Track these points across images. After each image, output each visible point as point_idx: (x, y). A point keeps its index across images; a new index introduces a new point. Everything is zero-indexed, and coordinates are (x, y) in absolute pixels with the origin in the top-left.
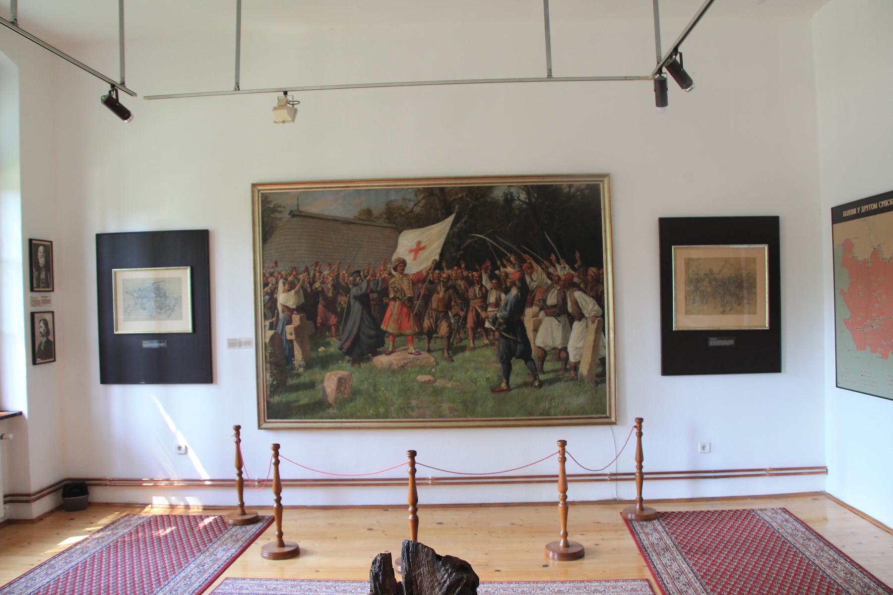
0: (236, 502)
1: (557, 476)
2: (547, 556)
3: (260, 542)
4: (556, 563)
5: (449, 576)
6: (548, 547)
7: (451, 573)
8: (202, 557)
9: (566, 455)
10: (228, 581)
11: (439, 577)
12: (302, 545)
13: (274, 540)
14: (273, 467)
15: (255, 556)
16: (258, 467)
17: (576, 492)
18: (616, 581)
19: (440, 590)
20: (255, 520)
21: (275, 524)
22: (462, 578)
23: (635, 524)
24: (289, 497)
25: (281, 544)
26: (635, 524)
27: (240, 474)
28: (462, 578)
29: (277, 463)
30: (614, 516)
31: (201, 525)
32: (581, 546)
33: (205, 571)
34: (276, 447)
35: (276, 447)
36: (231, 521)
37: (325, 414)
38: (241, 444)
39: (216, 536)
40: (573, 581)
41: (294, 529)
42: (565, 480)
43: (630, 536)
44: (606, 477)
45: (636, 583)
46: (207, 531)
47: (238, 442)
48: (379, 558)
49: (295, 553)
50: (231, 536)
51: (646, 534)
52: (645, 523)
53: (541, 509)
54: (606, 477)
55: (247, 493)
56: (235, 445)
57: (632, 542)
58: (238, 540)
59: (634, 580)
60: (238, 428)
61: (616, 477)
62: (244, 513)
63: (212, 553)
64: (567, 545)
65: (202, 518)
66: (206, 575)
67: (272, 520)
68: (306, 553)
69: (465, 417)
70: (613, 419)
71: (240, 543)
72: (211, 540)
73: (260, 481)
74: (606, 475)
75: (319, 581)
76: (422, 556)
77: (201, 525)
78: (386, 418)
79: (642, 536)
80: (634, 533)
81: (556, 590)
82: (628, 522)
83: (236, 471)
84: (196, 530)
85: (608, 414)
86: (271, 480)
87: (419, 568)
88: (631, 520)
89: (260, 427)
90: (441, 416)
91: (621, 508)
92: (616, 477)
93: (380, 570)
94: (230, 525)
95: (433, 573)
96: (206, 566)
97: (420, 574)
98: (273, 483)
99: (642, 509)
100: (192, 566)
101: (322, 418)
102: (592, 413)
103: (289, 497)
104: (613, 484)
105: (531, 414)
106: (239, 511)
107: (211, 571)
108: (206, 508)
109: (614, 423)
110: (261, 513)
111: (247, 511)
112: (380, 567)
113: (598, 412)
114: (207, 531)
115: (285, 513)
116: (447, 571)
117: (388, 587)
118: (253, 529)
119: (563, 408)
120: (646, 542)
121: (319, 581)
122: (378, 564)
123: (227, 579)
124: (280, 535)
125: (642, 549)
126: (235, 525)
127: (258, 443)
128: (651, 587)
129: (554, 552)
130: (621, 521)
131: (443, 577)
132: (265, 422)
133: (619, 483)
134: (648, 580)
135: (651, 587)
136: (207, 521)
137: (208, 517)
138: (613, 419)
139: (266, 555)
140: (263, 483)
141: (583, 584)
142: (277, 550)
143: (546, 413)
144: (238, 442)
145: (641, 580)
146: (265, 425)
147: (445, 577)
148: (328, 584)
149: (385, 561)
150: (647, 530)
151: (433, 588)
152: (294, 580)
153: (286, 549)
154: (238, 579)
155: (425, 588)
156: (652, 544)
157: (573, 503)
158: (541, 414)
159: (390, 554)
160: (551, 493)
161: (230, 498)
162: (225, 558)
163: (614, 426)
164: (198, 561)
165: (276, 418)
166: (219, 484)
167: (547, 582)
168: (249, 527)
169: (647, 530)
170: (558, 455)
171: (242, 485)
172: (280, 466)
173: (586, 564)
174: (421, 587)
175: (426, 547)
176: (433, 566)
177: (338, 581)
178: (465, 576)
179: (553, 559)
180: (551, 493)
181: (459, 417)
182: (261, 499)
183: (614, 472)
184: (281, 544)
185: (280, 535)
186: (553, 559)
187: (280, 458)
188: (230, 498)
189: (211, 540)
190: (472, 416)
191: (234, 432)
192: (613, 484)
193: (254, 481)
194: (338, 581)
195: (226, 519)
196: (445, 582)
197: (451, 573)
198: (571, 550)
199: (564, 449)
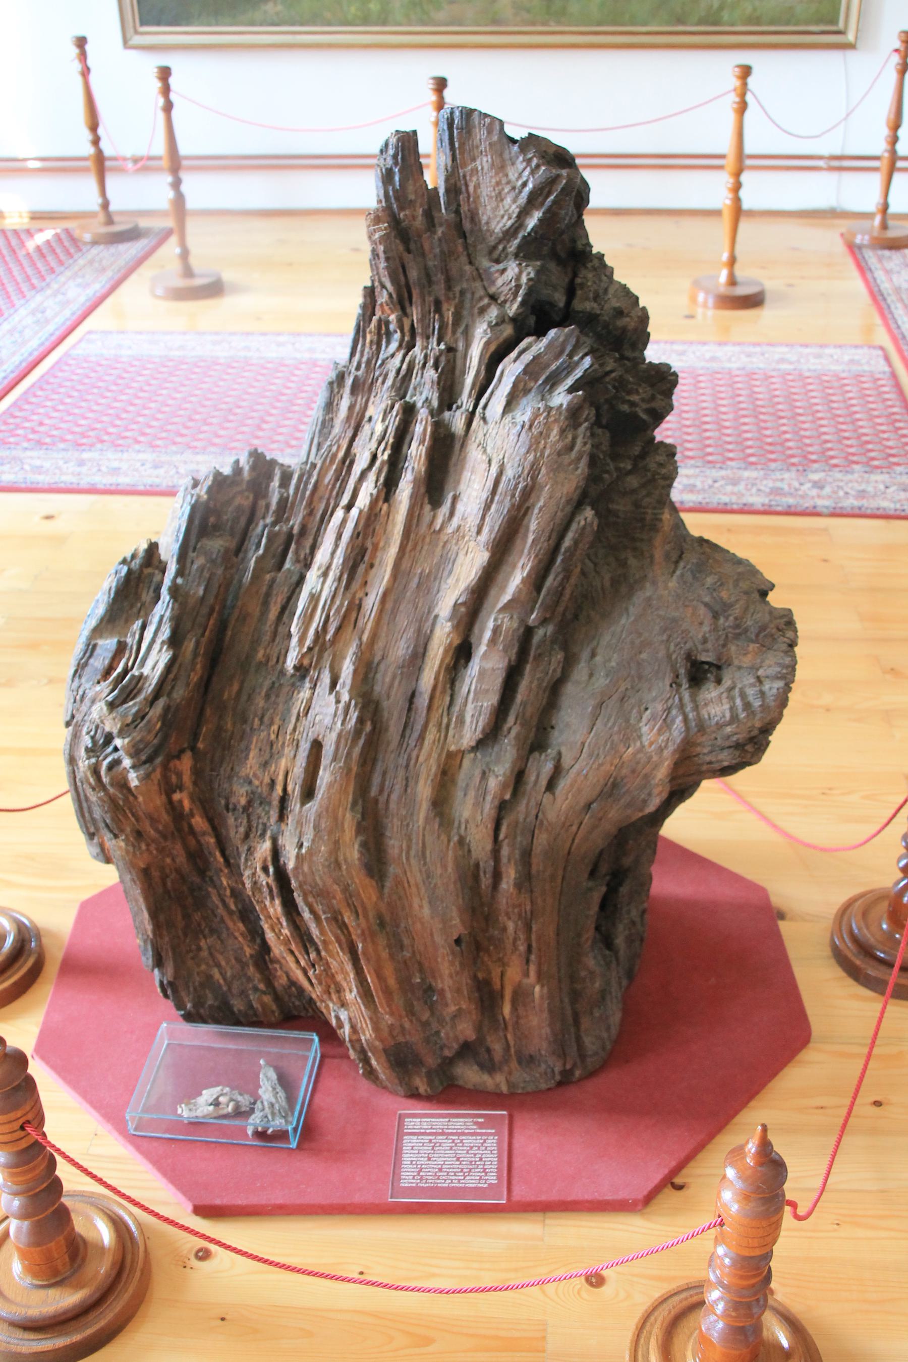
0: (92, 202)
1: (722, 157)
2: (693, 300)
3: (145, 272)
4: (710, 313)
5: (532, 172)
6: (697, 284)
7: (538, 167)
8: (39, 298)
9: (749, 98)
10: (92, 336)
11: (512, 175)
12: (228, 276)
13: (175, 266)
14: (161, 116)
15: (137, 294)
16: (132, 129)
17: (759, 191)
18: (822, 346)
19: (514, 201)
20: (132, 235)
21: (174, 240)
22: (558, 176)
23: (871, 257)
24: (200, 190)
25: (188, 272)
26: (871, 257)
27: (96, 141)
28: (558, 176)
29: (168, 107)
30: (828, 241)
31: (31, 245)
32: (761, 284)
33: (47, 321)
34: (165, 74)
35: (165, 74)
36: (87, 237)
37: (258, 15)
38: (92, 78)
39: (61, 263)
40: (739, 344)
41: (208, 247)
42: (742, 163)
43: (856, 273)
44: (821, 163)
45: (860, 351)
46: (43, 256)
47: (86, 72)
48: (393, 141)
49: (214, 289)
50: (91, 262)
51: (888, 272)
52: (887, 253)
53: (686, 222)
54: (821, 163)
55: (112, 182)
56: (79, 80)
57: (857, 285)
58: (104, 270)
59: (856, 347)
60: (81, 42)
61: (840, 163)
62: (110, 221)
63: (58, 291)
64: (732, 281)
65: (30, 233)
66: (51, 328)
67: (168, 233)
68: (236, 289)
69: (544, 24)
70: (851, 37)
71: (109, 273)
72: (52, 271)
73: (136, 160)
74: (820, 158)
75: (264, 334)
76: (480, 134)
77: (31, 245)
78: (384, 23)
79: (880, 275)
80: (863, 269)
81: (708, 356)
82: (853, 249)
83: (87, 136)
84: (21, 254)
85: (841, 25)
86: (159, 158)
87: (474, 159)
88: (860, 247)
89: (126, 44)
90: (495, 22)
91: (844, 225)
92: (840, 163)
93: (396, 164)
94: (85, 243)
95: (501, 167)
96: (49, 314)
97: (475, 171)
98: (165, 163)
99: (884, 226)
100: (22, 312)
101: (252, 23)
102: (808, 22)
103: (200, 190)
104: (834, 176)
105: (680, 21)
106: (101, 217)
107: (60, 320)
108: (36, 216)
109: (851, 46)
110: (143, 223)
111: (116, 219)
112: (395, 157)
113: (819, 21)
114: (43, 256)
115: (192, 226)
116: (529, 161)
117: (412, 197)
118: (130, 250)
119: (749, 9)
120: (885, 286)
121: (264, 334)
122: (391, 152)
123: (90, 332)
124: (185, 255)
125: (877, 297)
126: (95, 243)
127: (125, 76)
128: (887, 359)
129: (707, 292)
130: (840, 247)
131: (520, 175)
132: (136, 32)
133: (846, 175)
134: (882, 348)
135: (887, 359)
136: (40, 239)
137: (41, 230)
138: (851, 37)
139: (160, 292)
140: (144, 164)
141: (758, 349)
142: (181, 283)
143: (712, 19)
144: (86, 72)
145: (870, 347)
146: (137, 40)
147: (524, 175)
148: (281, 339)
149: (407, 143)
150: (889, 265)
151: (500, 198)
152: (216, 333)
153: (198, 282)
154: (111, 332)
155: (484, 199)
156: (898, 290)
157: (751, 213)
158: (700, 22)
159: (415, 132)
160: (712, 191)
161: (81, 194)
162: (82, 299)
163: (850, 54)
164: (33, 305)
165: (158, 24)
166: (58, 166)
167: (691, 343)
168: (122, 247)
169: (889, 265)
170: (733, 98)
171: (101, 165)
172: (175, 113)
173: (766, 315)
174: (477, 197)
175: (486, 115)
176: (501, 155)
177: (299, 334)
178: (564, 172)
179: (705, 305)
180: (712, 191)
181: (533, 24)
182: (140, 195)
183: (838, 152)
184: (188, 272)
185: (185, 255)
186: (705, 305)
187: (173, 97)
188: (81, 194)
189: (52, 271)
190: (559, 23)
191: (75, 51)
192: (830, 178)
193: (125, 159)
194: (299, 334)
195: (77, 233)
196: (525, 184)
197: (538, 167)
198: (741, 291)
199: (745, 85)
